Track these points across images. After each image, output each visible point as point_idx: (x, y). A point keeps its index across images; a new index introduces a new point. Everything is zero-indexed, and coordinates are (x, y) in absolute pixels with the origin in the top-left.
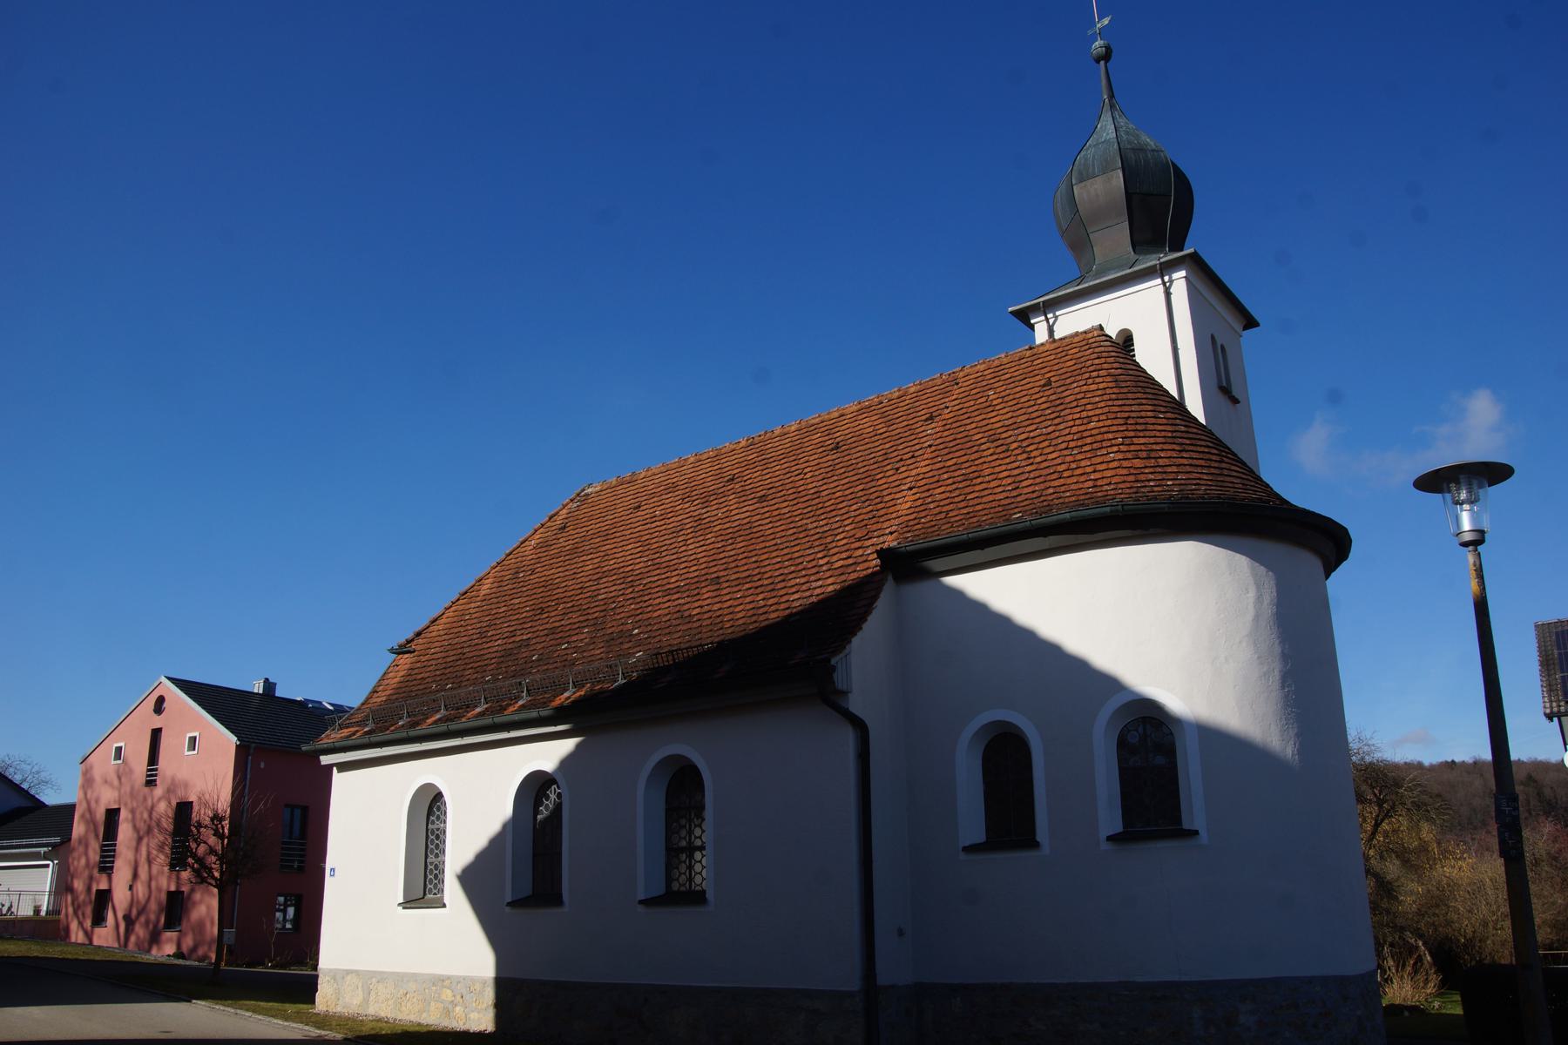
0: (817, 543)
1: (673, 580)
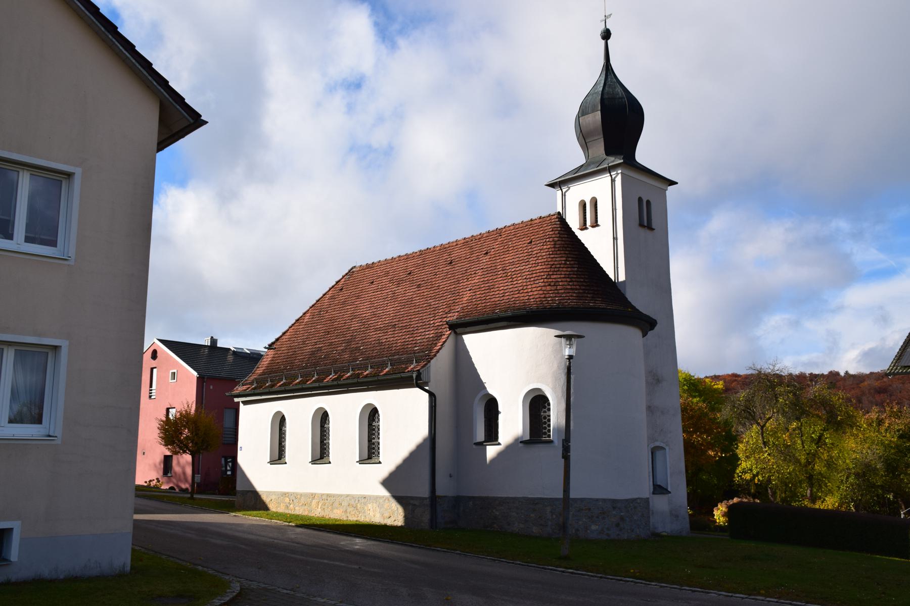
0: (432, 313)
1: (379, 324)
